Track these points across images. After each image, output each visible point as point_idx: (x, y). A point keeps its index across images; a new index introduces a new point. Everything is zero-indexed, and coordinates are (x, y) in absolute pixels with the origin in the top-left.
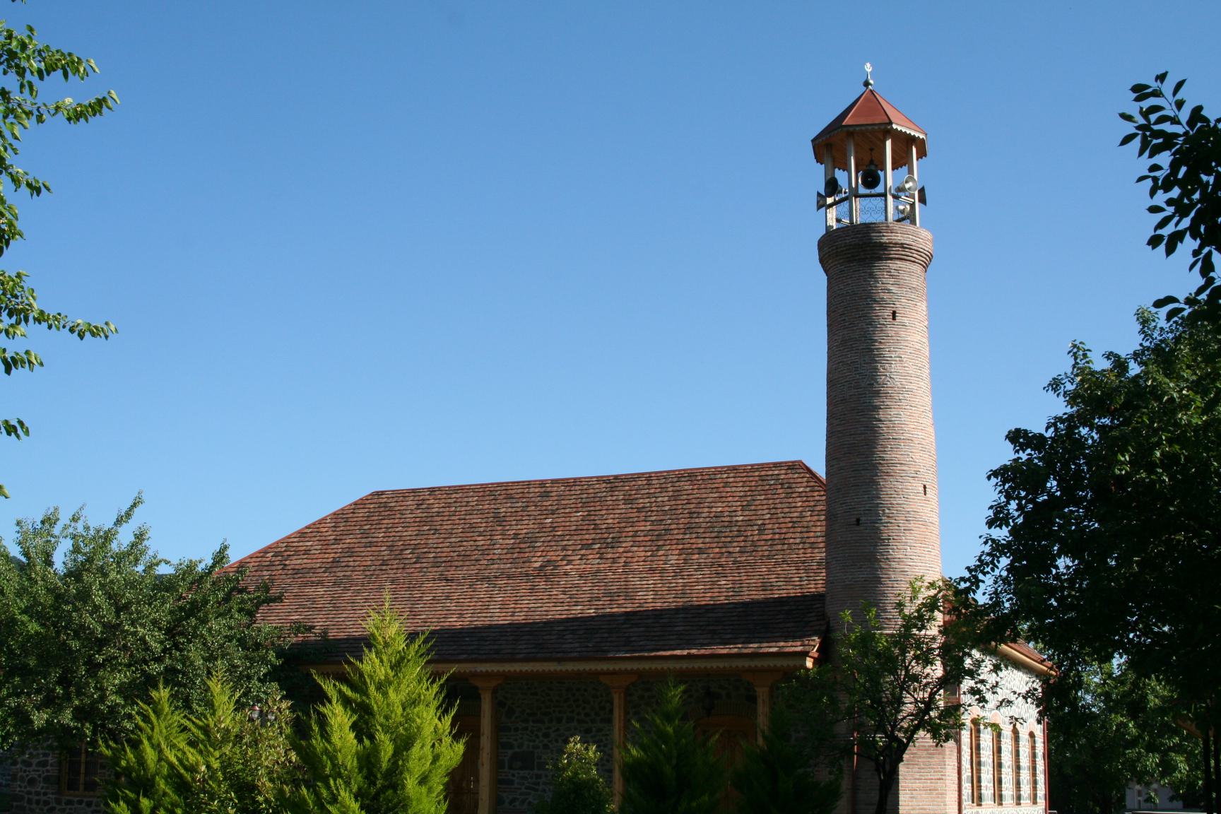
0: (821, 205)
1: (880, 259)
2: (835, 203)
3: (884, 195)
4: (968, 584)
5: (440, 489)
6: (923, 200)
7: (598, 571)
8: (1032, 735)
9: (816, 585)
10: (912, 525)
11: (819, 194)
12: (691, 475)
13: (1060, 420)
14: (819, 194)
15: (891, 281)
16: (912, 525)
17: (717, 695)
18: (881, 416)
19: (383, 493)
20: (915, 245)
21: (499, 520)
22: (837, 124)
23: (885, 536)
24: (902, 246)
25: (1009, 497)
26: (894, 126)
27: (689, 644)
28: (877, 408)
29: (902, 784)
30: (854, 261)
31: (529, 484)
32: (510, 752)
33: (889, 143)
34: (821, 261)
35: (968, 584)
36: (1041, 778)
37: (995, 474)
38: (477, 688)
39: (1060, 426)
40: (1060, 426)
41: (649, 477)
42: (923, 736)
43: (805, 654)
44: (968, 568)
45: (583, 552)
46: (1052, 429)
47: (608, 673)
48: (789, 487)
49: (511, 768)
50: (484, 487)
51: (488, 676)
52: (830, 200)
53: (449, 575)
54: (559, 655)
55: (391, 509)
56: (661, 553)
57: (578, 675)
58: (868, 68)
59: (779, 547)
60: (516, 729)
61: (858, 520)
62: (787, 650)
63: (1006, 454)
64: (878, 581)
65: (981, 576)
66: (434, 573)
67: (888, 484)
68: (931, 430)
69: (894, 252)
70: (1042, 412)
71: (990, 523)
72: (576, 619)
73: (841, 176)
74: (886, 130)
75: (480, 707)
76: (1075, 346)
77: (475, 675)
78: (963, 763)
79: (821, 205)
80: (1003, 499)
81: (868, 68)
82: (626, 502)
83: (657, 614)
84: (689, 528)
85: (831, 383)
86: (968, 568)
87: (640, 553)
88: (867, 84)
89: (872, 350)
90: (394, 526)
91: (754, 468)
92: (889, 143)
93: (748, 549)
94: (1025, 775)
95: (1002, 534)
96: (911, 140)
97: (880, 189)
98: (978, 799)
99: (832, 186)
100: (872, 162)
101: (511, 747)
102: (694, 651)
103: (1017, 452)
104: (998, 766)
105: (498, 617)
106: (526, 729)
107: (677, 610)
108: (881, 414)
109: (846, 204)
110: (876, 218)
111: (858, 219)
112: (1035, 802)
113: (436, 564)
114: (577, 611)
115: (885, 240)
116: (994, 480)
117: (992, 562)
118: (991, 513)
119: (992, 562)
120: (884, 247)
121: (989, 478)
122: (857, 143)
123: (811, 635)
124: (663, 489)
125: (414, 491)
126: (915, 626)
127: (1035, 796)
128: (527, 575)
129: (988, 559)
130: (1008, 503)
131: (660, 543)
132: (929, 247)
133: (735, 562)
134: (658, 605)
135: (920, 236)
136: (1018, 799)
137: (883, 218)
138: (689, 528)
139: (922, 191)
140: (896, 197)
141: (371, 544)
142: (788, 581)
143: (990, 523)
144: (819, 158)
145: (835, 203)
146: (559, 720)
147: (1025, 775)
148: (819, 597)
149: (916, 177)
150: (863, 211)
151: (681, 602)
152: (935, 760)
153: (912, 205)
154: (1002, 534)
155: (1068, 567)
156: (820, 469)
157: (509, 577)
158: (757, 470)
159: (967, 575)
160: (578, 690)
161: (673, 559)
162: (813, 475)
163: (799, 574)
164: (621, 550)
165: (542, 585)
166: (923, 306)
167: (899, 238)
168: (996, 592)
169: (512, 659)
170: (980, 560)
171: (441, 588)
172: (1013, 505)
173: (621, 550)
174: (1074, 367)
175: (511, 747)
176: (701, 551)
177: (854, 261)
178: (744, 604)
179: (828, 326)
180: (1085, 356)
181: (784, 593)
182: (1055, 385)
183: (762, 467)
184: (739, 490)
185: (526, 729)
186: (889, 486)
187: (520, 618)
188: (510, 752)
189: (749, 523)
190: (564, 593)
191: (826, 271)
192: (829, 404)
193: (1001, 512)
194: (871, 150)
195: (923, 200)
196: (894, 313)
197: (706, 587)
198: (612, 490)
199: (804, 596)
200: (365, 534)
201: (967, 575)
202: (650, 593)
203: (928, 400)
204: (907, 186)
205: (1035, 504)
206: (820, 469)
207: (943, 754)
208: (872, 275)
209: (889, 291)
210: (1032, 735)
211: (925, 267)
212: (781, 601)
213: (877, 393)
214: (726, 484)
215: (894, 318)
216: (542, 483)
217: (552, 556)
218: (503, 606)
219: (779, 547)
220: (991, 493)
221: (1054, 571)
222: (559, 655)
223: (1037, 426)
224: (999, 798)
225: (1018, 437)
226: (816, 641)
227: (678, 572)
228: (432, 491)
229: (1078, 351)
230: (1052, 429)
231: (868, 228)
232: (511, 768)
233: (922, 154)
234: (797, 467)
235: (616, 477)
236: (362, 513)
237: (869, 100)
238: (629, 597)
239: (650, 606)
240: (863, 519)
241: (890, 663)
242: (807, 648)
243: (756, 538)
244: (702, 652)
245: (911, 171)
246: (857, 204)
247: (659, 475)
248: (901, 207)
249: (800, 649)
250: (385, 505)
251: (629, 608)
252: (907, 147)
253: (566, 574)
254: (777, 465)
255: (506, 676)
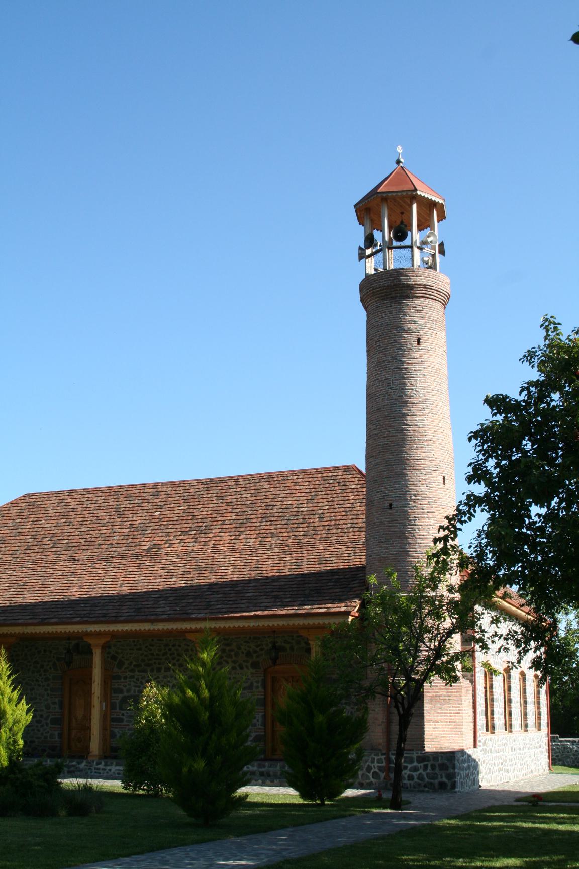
0: (362, 256)
1: (408, 297)
2: (373, 254)
3: (411, 247)
4: (446, 532)
5: (76, 491)
6: (442, 252)
7: (192, 551)
8: (523, 674)
9: (359, 560)
10: (433, 509)
11: (360, 248)
12: (269, 477)
13: (530, 384)
14: (360, 248)
15: (417, 314)
16: (433, 509)
17: (275, 650)
18: (409, 422)
19: (33, 495)
20: (436, 287)
21: (120, 514)
22: (374, 192)
23: (412, 517)
24: (425, 286)
25: (488, 454)
26: (419, 193)
27: (257, 607)
28: (406, 415)
29: (427, 717)
30: (387, 297)
31: (144, 486)
32: (121, 696)
33: (414, 207)
34: (362, 300)
35: (446, 532)
36: (544, 710)
37: (475, 435)
38: (90, 645)
39: (533, 389)
40: (533, 389)
41: (237, 479)
42: (436, 681)
43: (348, 613)
44: (447, 518)
45: (182, 537)
46: (525, 393)
47: (192, 631)
48: (344, 484)
49: (121, 708)
50: (110, 489)
51: (99, 634)
52: (369, 252)
53: (77, 556)
54: (153, 617)
55: (38, 507)
56: (242, 537)
57: (170, 632)
58: (400, 150)
59: (334, 531)
60: (125, 678)
61: (391, 505)
62: (333, 610)
63: (485, 416)
64: (407, 553)
65: (459, 525)
66: (65, 555)
67: (414, 476)
68: (450, 433)
69: (418, 292)
70: (515, 379)
71: (470, 479)
72: (171, 589)
73: (377, 235)
74: (412, 196)
75: (92, 659)
76: (546, 320)
77: (88, 634)
78: (478, 699)
79: (362, 256)
80: (481, 457)
81: (400, 150)
82: (219, 498)
83: (234, 584)
84: (265, 517)
85: (370, 396)
86: (447, 518)
87: (226, 537)
88: (398, 162)
89: (401, 369)
90: (39, 519)
91: (318, 471)
92: (414, 207)
93: (310, 533)
94: (531, 708)
95: (480, 489)
96: (432, 205)
97: (407, 242)
98: (490, 727)
99: (370, 241)
100: (402, 223)
101: (121, 691)
102: (260, 613)
103: (495, 415)
104: (508, 701)
105: (110, 589)
106: (132, 677)
107: (249, 581)
108: (409, 420)
109: (381, 255)
110: (405, 265)
111: (391, 266)
112: (539, 729)
113: (68, 549)
114: (172, 583)
115: (411, 282)
116: (474, 441)
117: (469, 512)
118: (470, 469)
119: (469, 512)
120: (411, 287)
121: (470, 439)
122: (391, 210)
123: (353, 599)
124: (247, 488)
125: (56, 493)
126: (429, 586)
127: (540, 724)
128: (137, 556)
129: (466, 509)
130: (486, 460)
131: (242, 529)
132: (447, 288)
133: (299, 543)
134: (236, 577)
135: (440, 280)
136: (509, 726)
137: (410, 265)
138: (265, 517)
139: (441, 245)
140: (420, 249)
141: (19, 534)
142: (339, 556)
143: (470, 479)
144: (361, 222)
145: (373, 254)
146: (159, 670)
147: (531, 708)
148: (361, 570)
149: (436, 233)
150: (394, 260)
151: (253, 575)
152: (454, 697)
153: (434, 256)
154: (480, 489)
155: (539, 515)
156: (363, 469)
157: (122, 557)
158: (321, 472)
159: (446, 523)
160: (174, 645)
161: (251, 542)
162: (360, 472)
163: (345, 552)
164: (211, 535)
165: (147, 563)
166: (442, 335)
167: (423, 281)
168: (480, 545)
169: (116, 621)
170: (457, 509)
171: (70, 566)
172: (491, 462)
173: (211, 535)
174: (546, 339)
175: (121, 691)
176: (273, 535)
177: (387, 297)
178: (303, 575)
179: (368, 351)
180: (556, 329)
181: (334, 566)
182: (530, 356)
183: (324, 470)
184: (305, 488)
185: (132, 677)
186: (414, 477)
187: (126, 589)
188: (121, 696)
189: (312, 513)
190: (163, 569)
191: (366, 308)
192: (368, 414)
193: (479, 469)
194: (402, 213)
195: (442, 252)
196: (419, 340)
197: (275, 563)
198: (208, 489)
199: (350, 569)
200: (16, 526)
201: (446, 523)
202: (230, 568)
203: (446, 409)
204: (429, 240)
205: (510, 461)
206: (363, 469)
207: (459, 691)
208: (401, 310)
209: (415, 322)
210: (523, 674)
211: (445, 304)
212: (332, 572)
213: (405, 404)
214: (296, 484)
215: (419, 344)
216: (155, 486)
217: (157, 541)
218: (115, 580)
219: (334, 531)
220: (471, 452)
221: (527, 521)
222: (153, 617)
223: (515, 394)
224: (509, 726)
225: (496, 403)
226: (357, 603)
227: (255, 551)
228: (70, 492)
229: (549, 325)
230: (525, 393)
231: (398, 272)
232: (121, 708)
233: (442, 217)
234: (348, 469)
235: (212, 480)
236: (15, 510)
237: (401, 173)
238: (214, 572)
239: (228, 578)
240: (394, 504)
241: (406, 618)
242: (349, 609)
243: (316, 524)
244: (266, 613)
245: (433, 229)
246: (391, 254)
247: (245, 478)
248: (426, 259)
249: (343, 609)
250: (34, 504)
251: (213, 579)
252: (431, 210)
253: (167, 554)
254: (335, 469)
255: (114, 635)
